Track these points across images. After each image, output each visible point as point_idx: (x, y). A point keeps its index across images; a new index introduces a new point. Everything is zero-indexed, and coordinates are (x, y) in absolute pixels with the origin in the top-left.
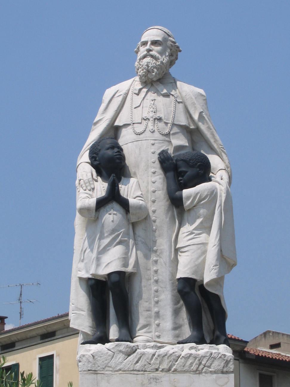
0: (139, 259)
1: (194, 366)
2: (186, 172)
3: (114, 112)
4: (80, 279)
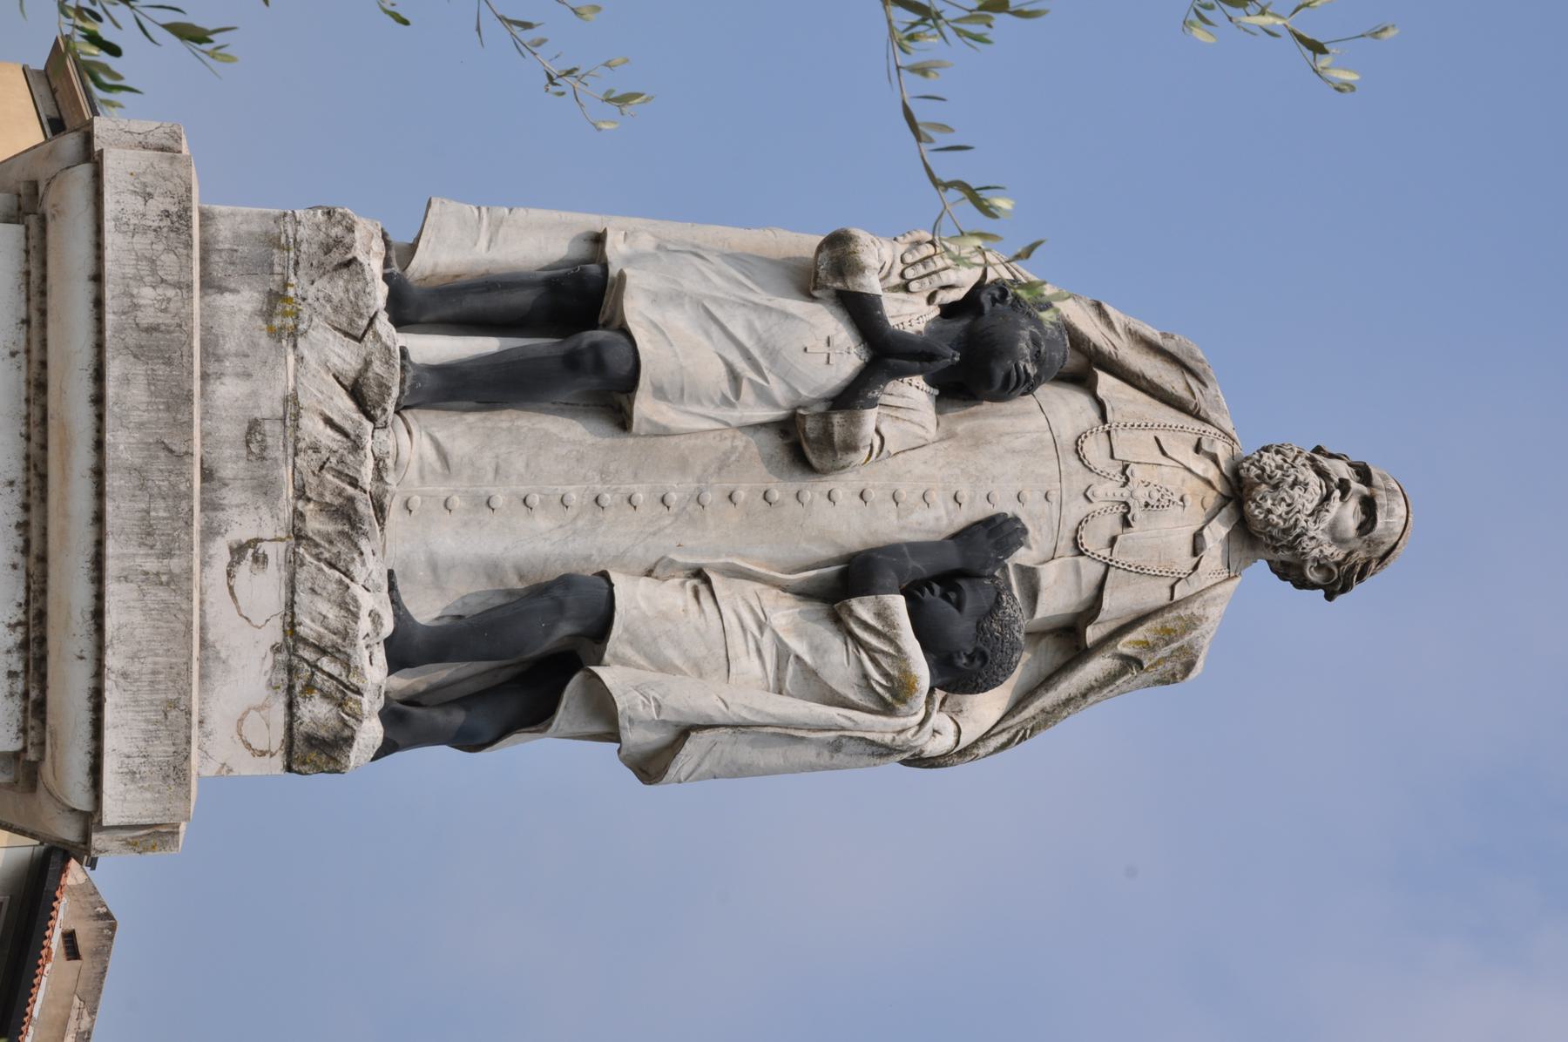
0: (673, 440)
2: (959, 606)
3: (1141, 371)
4: (598, 239)
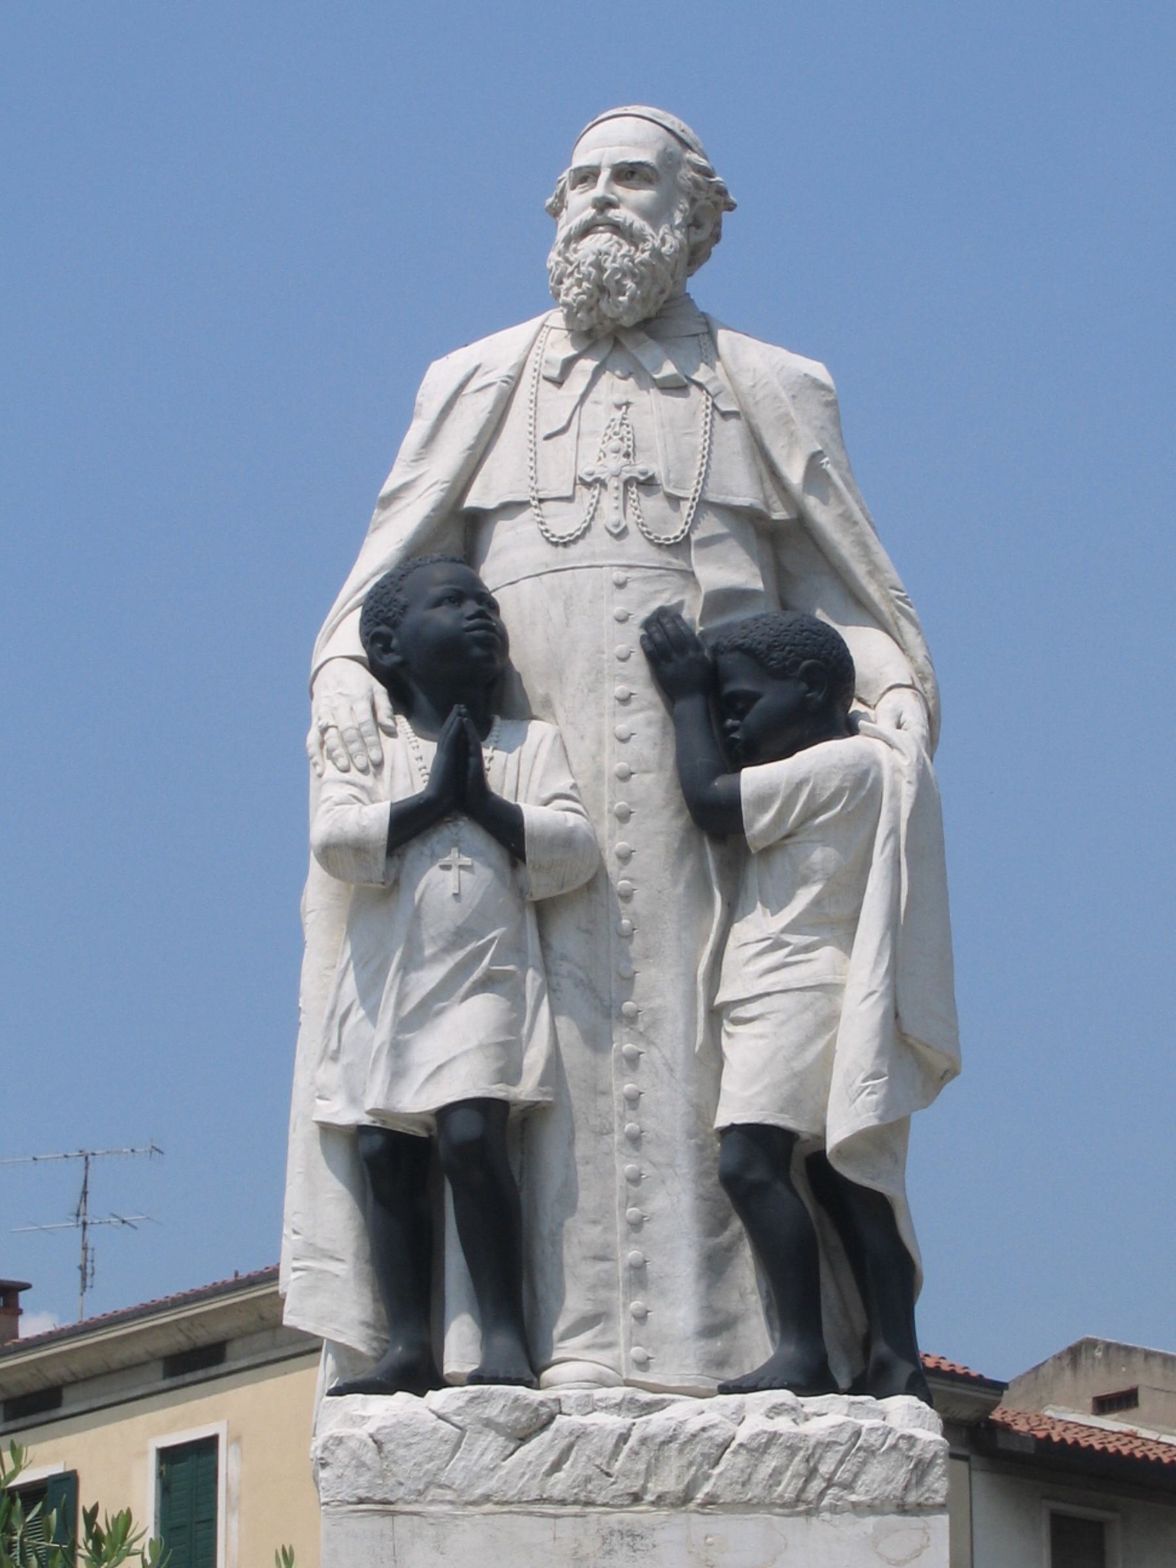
1: (788, 1485)
2: (754, 697)
3: (464, 452)
